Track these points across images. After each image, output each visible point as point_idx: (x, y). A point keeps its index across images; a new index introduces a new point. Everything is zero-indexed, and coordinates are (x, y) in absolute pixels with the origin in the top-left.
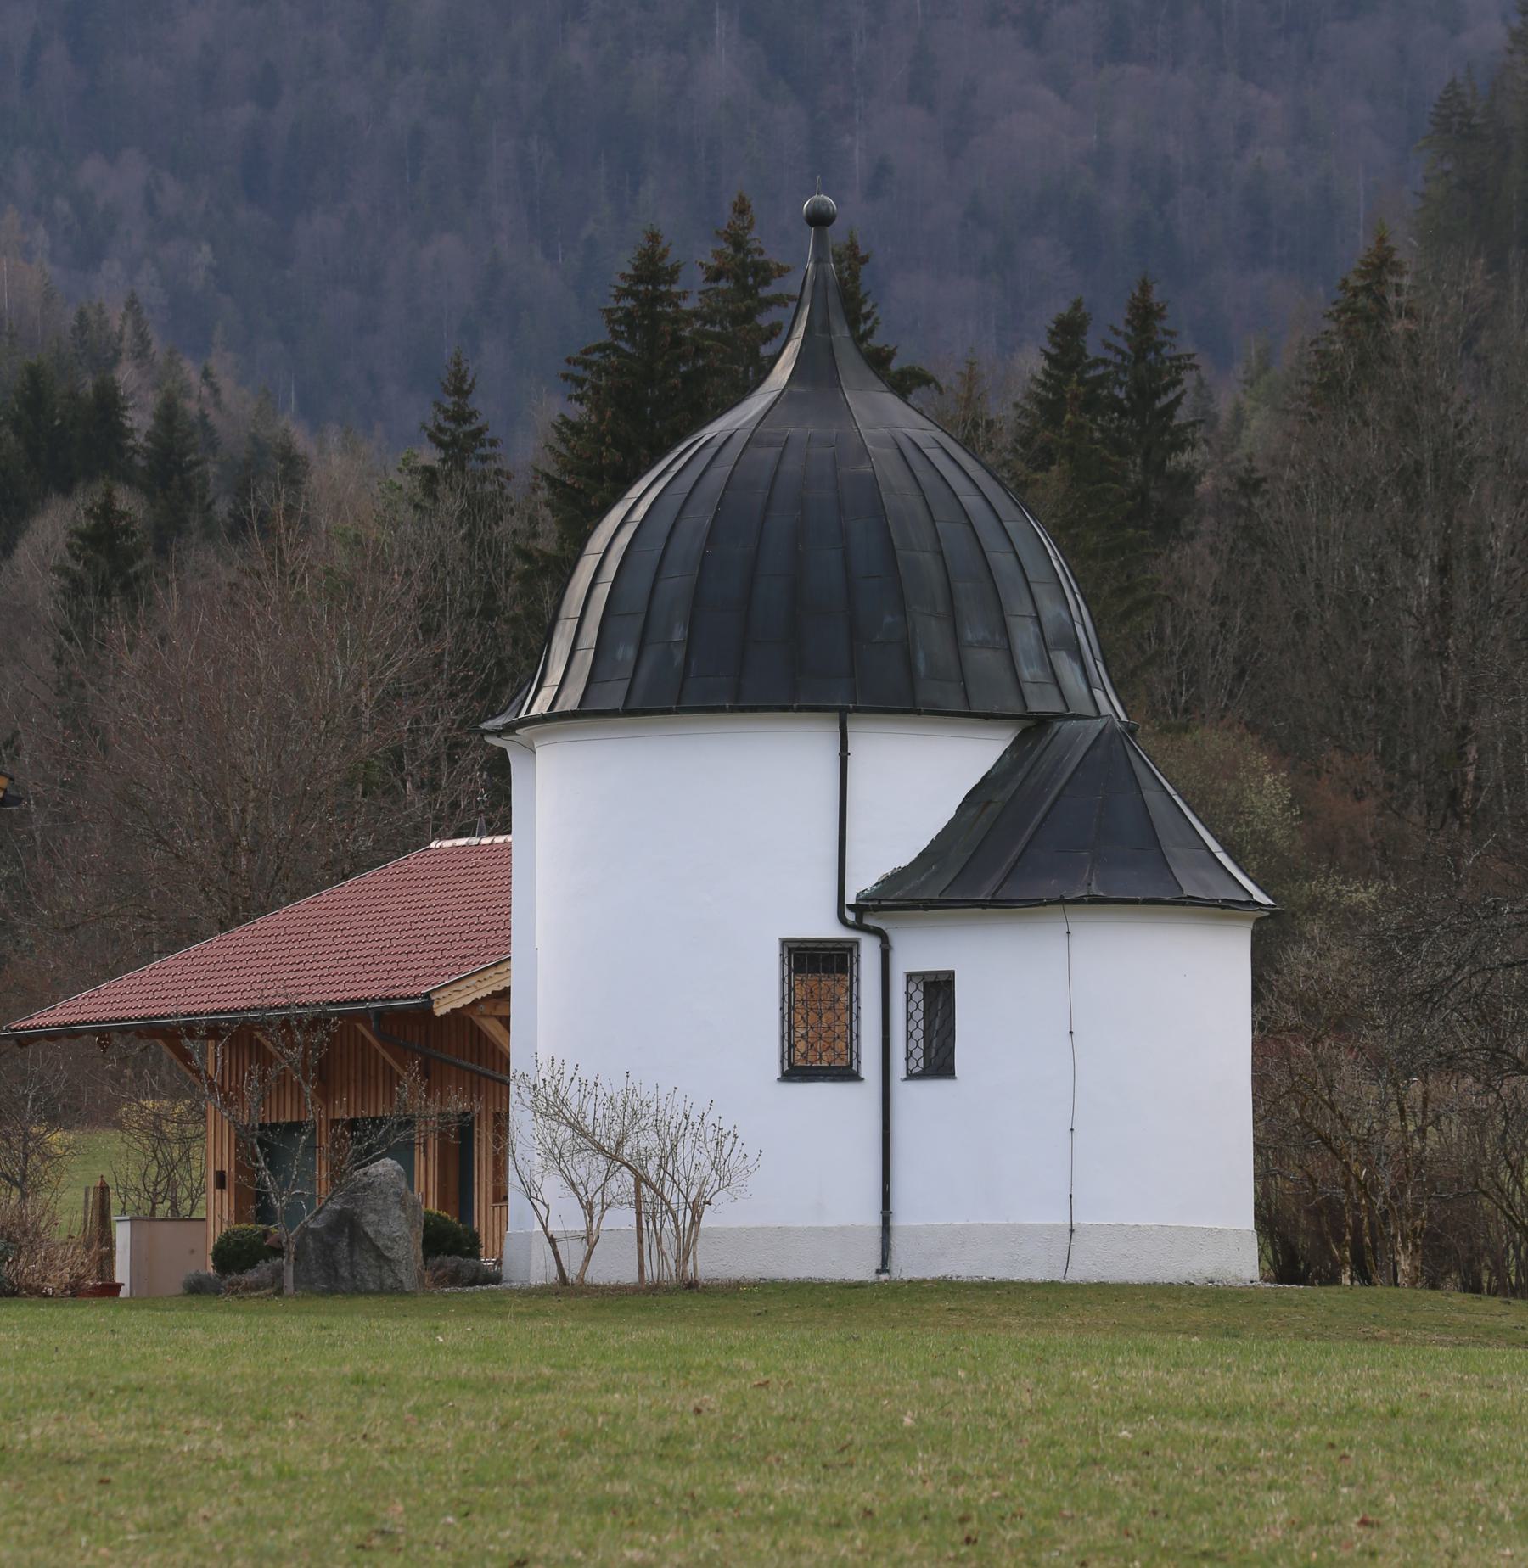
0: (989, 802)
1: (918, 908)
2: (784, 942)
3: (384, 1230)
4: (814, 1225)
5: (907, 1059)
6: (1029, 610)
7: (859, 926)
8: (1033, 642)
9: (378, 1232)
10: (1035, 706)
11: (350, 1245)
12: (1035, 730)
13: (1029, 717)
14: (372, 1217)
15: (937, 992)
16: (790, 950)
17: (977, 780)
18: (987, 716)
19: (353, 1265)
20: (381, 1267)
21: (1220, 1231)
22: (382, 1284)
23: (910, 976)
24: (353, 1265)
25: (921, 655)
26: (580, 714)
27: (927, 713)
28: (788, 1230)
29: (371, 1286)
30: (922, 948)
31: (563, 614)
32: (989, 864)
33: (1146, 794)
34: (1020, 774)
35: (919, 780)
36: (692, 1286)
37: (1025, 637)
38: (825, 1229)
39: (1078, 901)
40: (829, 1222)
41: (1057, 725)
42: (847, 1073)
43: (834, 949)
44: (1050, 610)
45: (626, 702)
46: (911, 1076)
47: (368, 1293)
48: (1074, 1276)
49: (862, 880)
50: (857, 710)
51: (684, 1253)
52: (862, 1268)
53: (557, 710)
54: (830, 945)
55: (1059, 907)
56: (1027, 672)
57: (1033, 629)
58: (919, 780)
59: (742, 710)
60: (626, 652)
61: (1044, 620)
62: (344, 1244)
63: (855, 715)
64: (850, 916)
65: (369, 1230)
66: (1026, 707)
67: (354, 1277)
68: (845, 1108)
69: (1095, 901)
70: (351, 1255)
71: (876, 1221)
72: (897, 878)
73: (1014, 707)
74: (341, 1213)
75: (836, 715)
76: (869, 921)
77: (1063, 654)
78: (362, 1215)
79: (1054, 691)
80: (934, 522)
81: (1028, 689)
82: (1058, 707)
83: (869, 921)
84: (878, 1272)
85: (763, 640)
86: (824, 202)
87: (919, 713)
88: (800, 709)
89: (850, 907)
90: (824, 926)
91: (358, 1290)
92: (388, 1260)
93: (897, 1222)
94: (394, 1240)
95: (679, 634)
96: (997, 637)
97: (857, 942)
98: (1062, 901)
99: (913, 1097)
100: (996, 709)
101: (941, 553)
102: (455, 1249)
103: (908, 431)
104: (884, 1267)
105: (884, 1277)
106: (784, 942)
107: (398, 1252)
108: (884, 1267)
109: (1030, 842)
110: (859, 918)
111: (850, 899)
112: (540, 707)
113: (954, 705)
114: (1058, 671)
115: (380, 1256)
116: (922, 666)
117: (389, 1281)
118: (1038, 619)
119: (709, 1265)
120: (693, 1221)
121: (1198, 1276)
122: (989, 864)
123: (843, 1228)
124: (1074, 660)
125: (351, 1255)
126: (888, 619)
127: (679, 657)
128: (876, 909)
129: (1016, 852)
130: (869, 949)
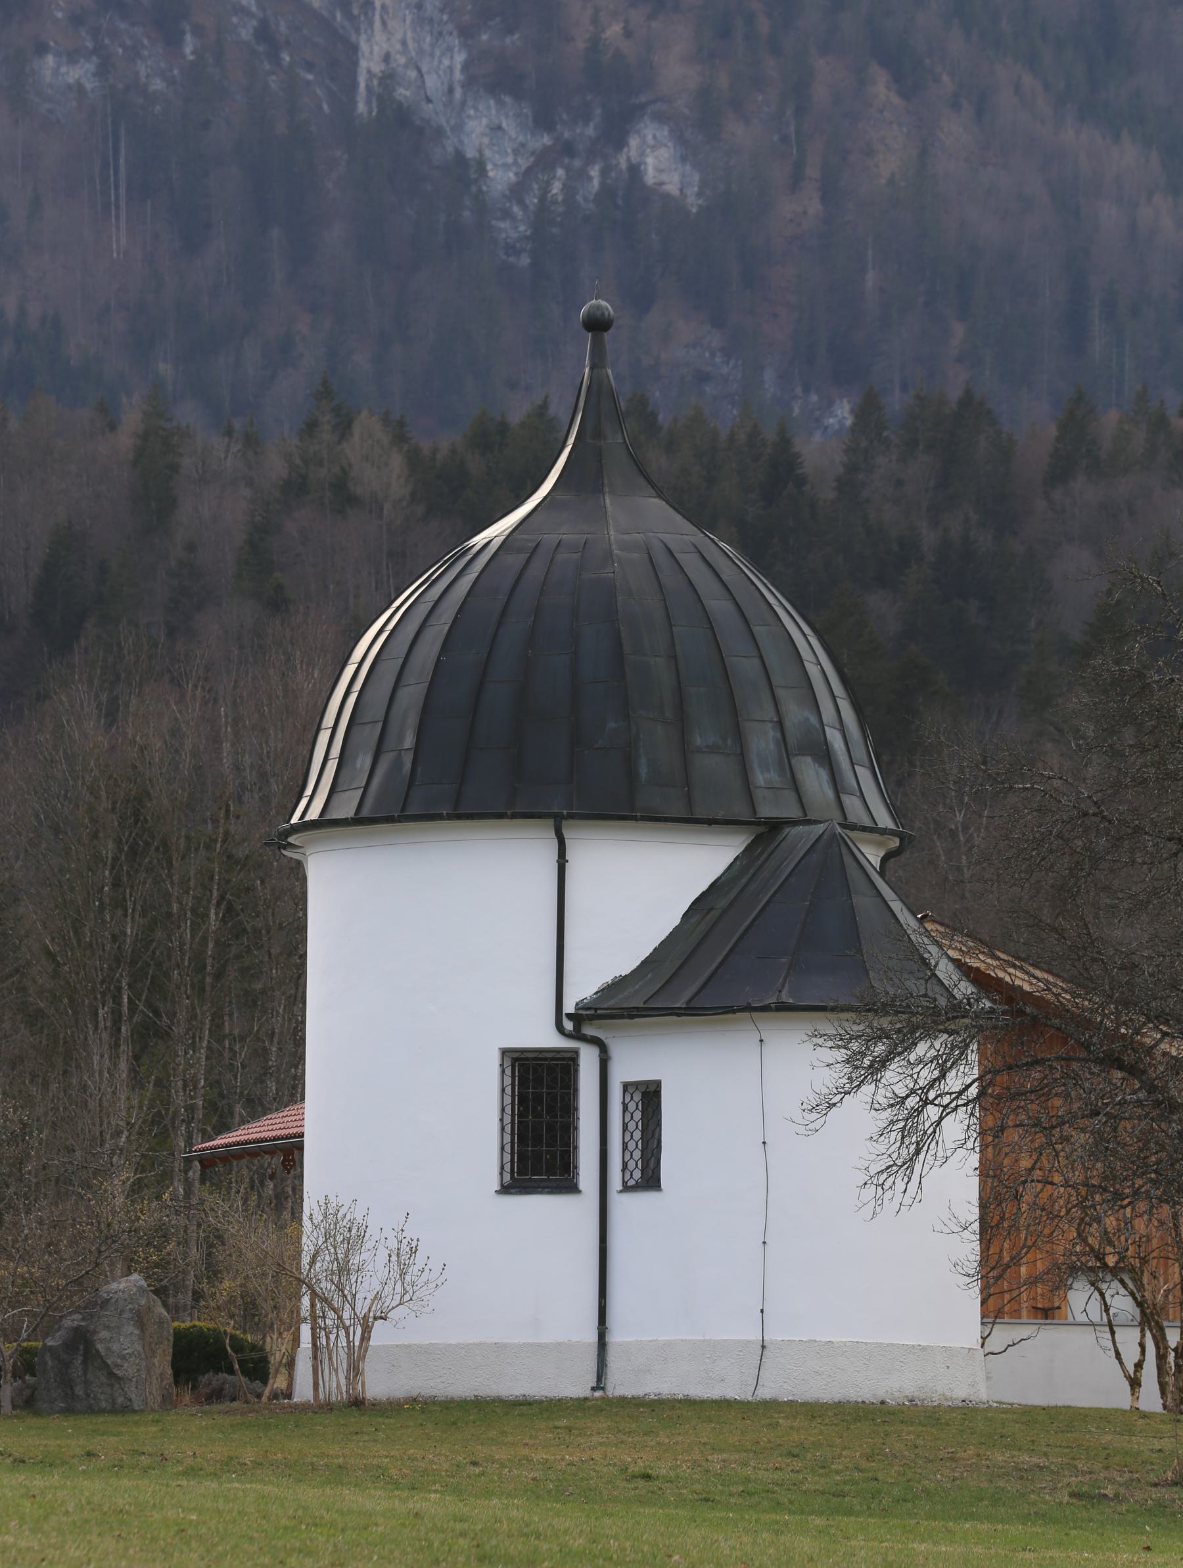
0: (711, 909)
1: (621, 1017)
2: (505, 1052)
3: (115, 1347)
4: (530, 1341)
5: (623, 1171)
6: (770, 714)
7: (577, 1035)
8: (772, 747)
9: (108, 1349)
10: (766, 811)
11: (84, 1362)
12: (767, 833)
13: (758, 823)
14: (104, 1334)
15: (649, 1096)
16: (514, 1060)
17: (704, 887)
18: (711, 822)
19: (87, 1383)
20: (112, 1386)
21: (924, 1349)
22: (114, 1403)
23: (626, 1086)
24: (87, 1383)
25: (643, 761)
26: (357, 821)
27: (643, 819)
28: (505, 1346)
29: (104, 1404)
30: (637, 1057)
31: (323, 726)
32: (707, 975)
33: (857, 900)
34: (744, 880)
35: (642, 887)
36: (357, 1403)
37: (762, 742)
38: (541, 1346)
39: (765, 1009)
40: (545, 1339)
41: (787, 830)
42: (570, 1186)
43: (553, 1059)
44: (795, 713)
45: (403, 810)
46: (626, 1188)
47: (102, 1411)
48: (765, 1393)
49: (581, 989)
50: (571, 816)
51: (355, 1370)
52: (575, 1383)
53: (306, 819)
54: (549, 1055)
55: (746, 1015)
56: (760, 778)
57: (772, 733)
58: (642, 887)
59: (459, 817)
60: (364, 762)
61: (788, 724)
62: (78, 1361)
63: (572, 822)
64: (569, 1025)
65: (99, 1346)
66: (755, 812)
67: (88, 1395)
68: (561, 1218)
69: (782, 1008)
70: (85, 1374)
71: (593, 1337)
72: (618, 984)
73: (740, 811)
74: (77, 1330)
75: (551, 822)
76: (588, 1031)
77: (809, 759)
78: (95, 1332)
79: (790, 796)
80: (671, 626)
81: (759, 794)
82: (794, 813)
83: (588, 1031)
84: (593, 1389)
85: (507, 749)
86: (599, 307)
87: (635, 819)
88: (514, 816)
89: (569, 1016)
90: (542, 1035)
91: (92, 1410)
92: (119, 1379)
93: (616, 1337)
94: (124, 1358)
95: (409, 741)
96: (729, 742)
97: (576, 1052)
98: (749, 1009)
99: (624, 1206)
100: (720, 815)
101: (675, 657)
102: (220, 1365)
103: (666, 537)
104: (599, 1385)
105: (598, 1394)
106: (505, 1052)
107: (128, 1369)
108: (599, 1385)
109: (731, 950)
110: (577, 1027)
111: (569, 1007)
112: (314, 814)
113: (686, 814)
114: (799, 776)
115: (111, 1374)
116: (643, 771)
117: (120, 1400)
118: (780, 724)
119: (378, 1384)
120: (362, 1339)
121: (897, 1394)
122: (707, 975)
123: (559, 1344)
124: (821, 765)
125: (85, 1374)
126: (612, 725)
127: (408, 766)
128: (591, 1018)
129: (719, 960)
130: (588, 1059)
